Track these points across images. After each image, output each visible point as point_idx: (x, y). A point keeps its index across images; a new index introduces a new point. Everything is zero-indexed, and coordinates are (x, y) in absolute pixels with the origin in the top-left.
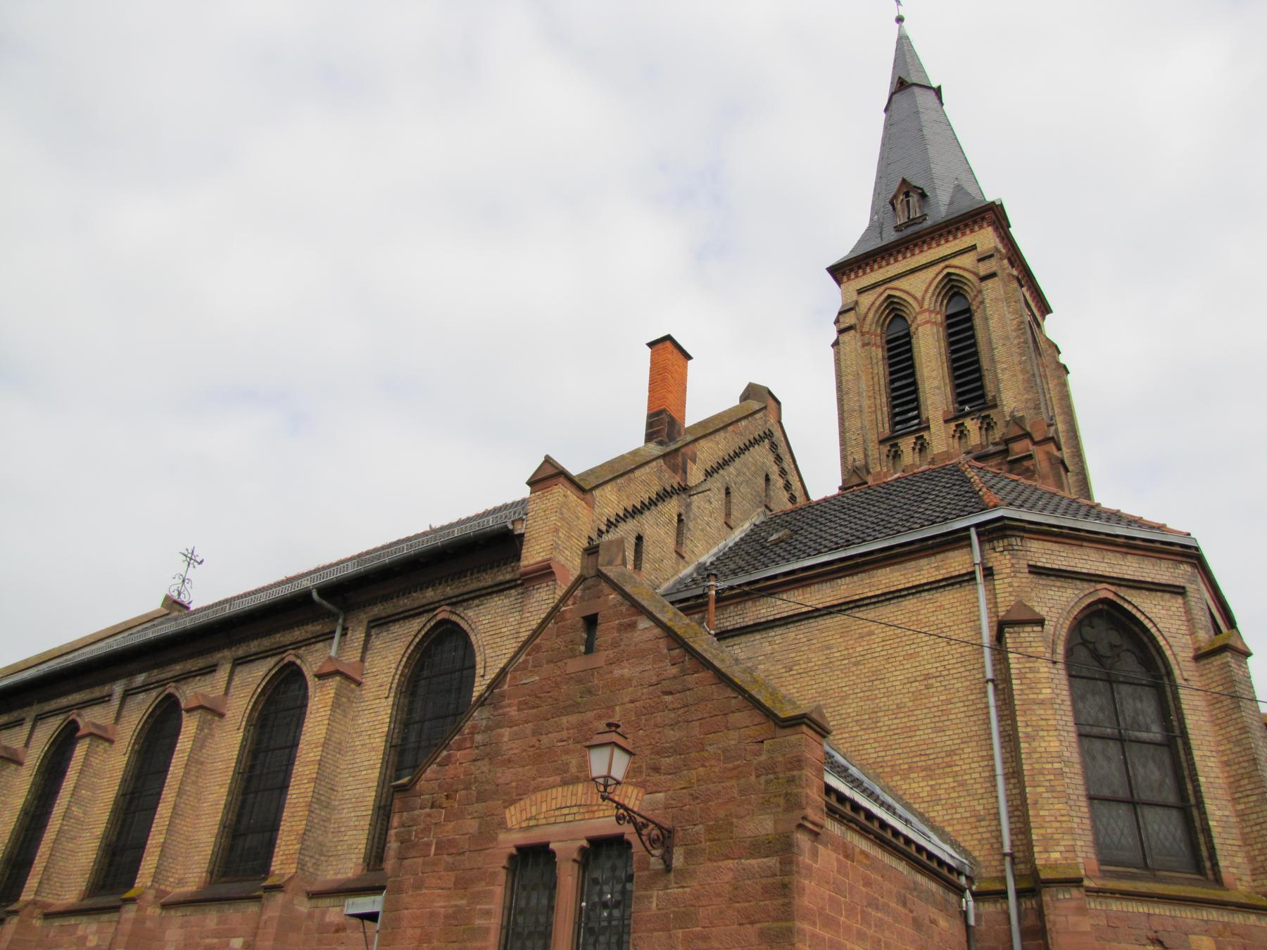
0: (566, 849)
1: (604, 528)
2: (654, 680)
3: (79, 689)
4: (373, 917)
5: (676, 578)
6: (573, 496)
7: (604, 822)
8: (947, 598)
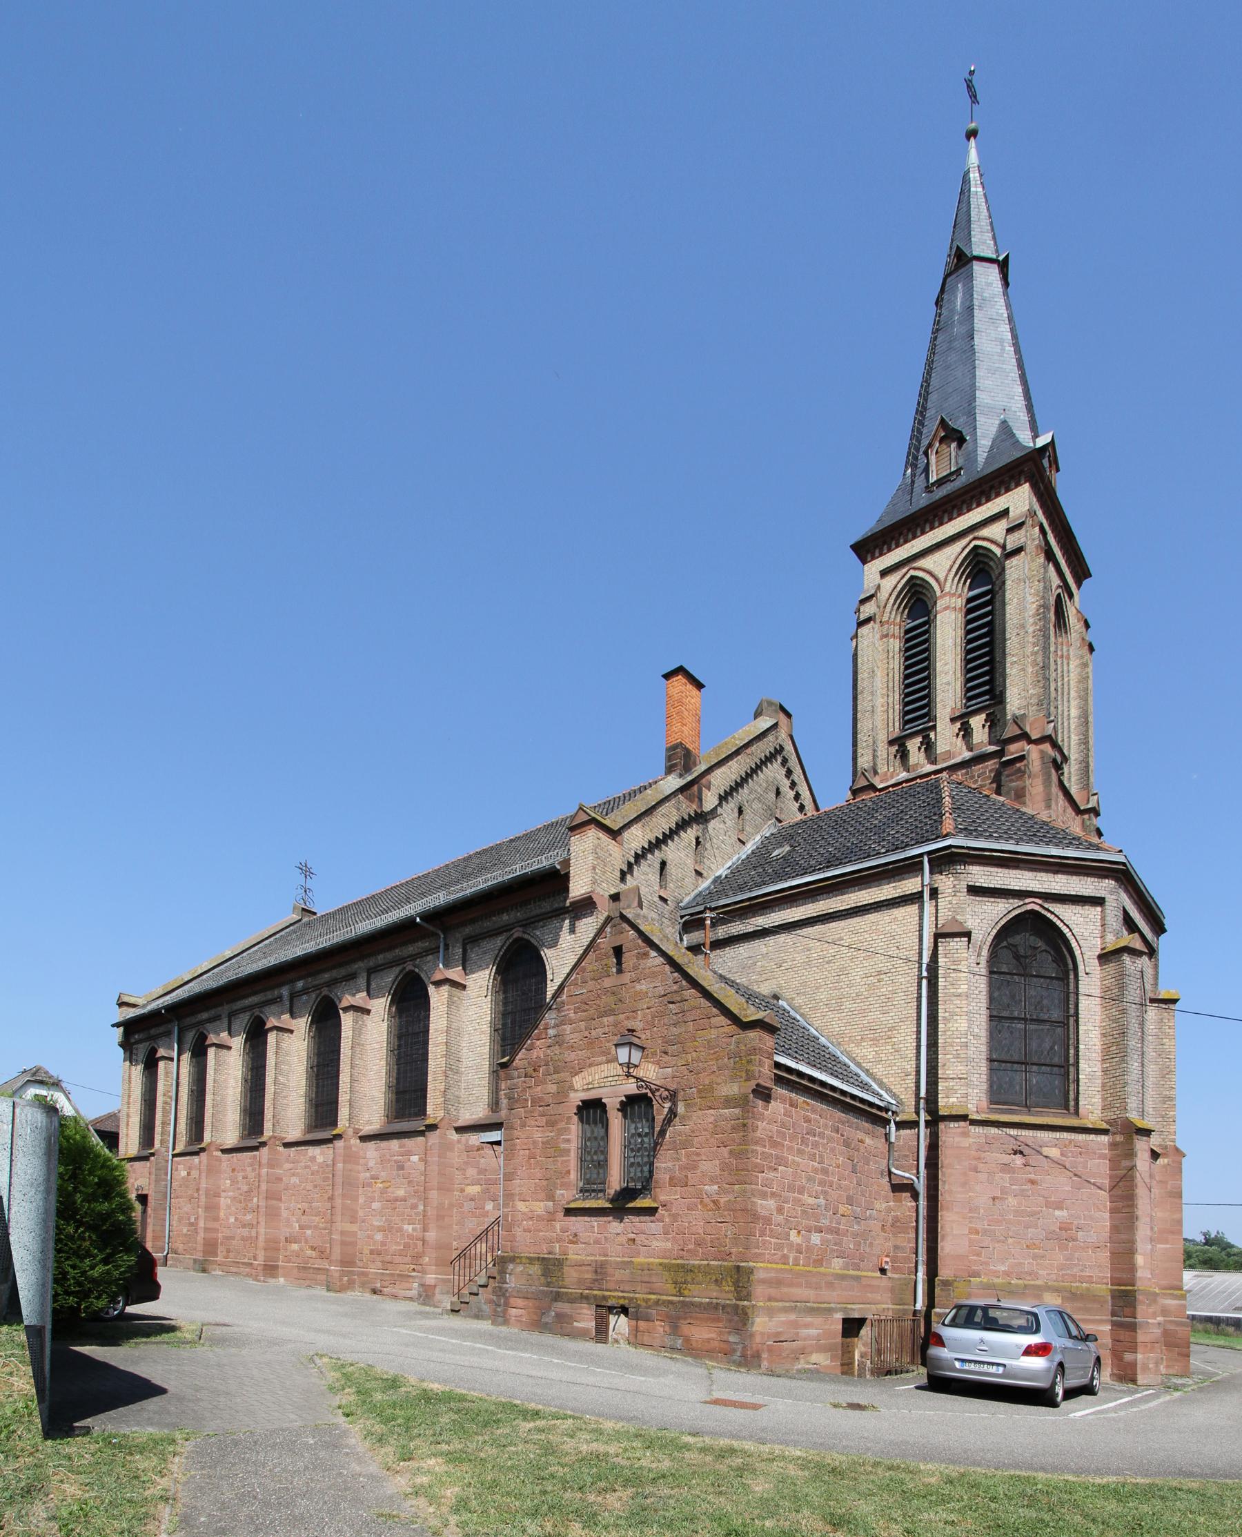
1: (632, 860)
3: (255, 993)
4: (498, 1143)
5: (696, 892)
7: (631, 1088)
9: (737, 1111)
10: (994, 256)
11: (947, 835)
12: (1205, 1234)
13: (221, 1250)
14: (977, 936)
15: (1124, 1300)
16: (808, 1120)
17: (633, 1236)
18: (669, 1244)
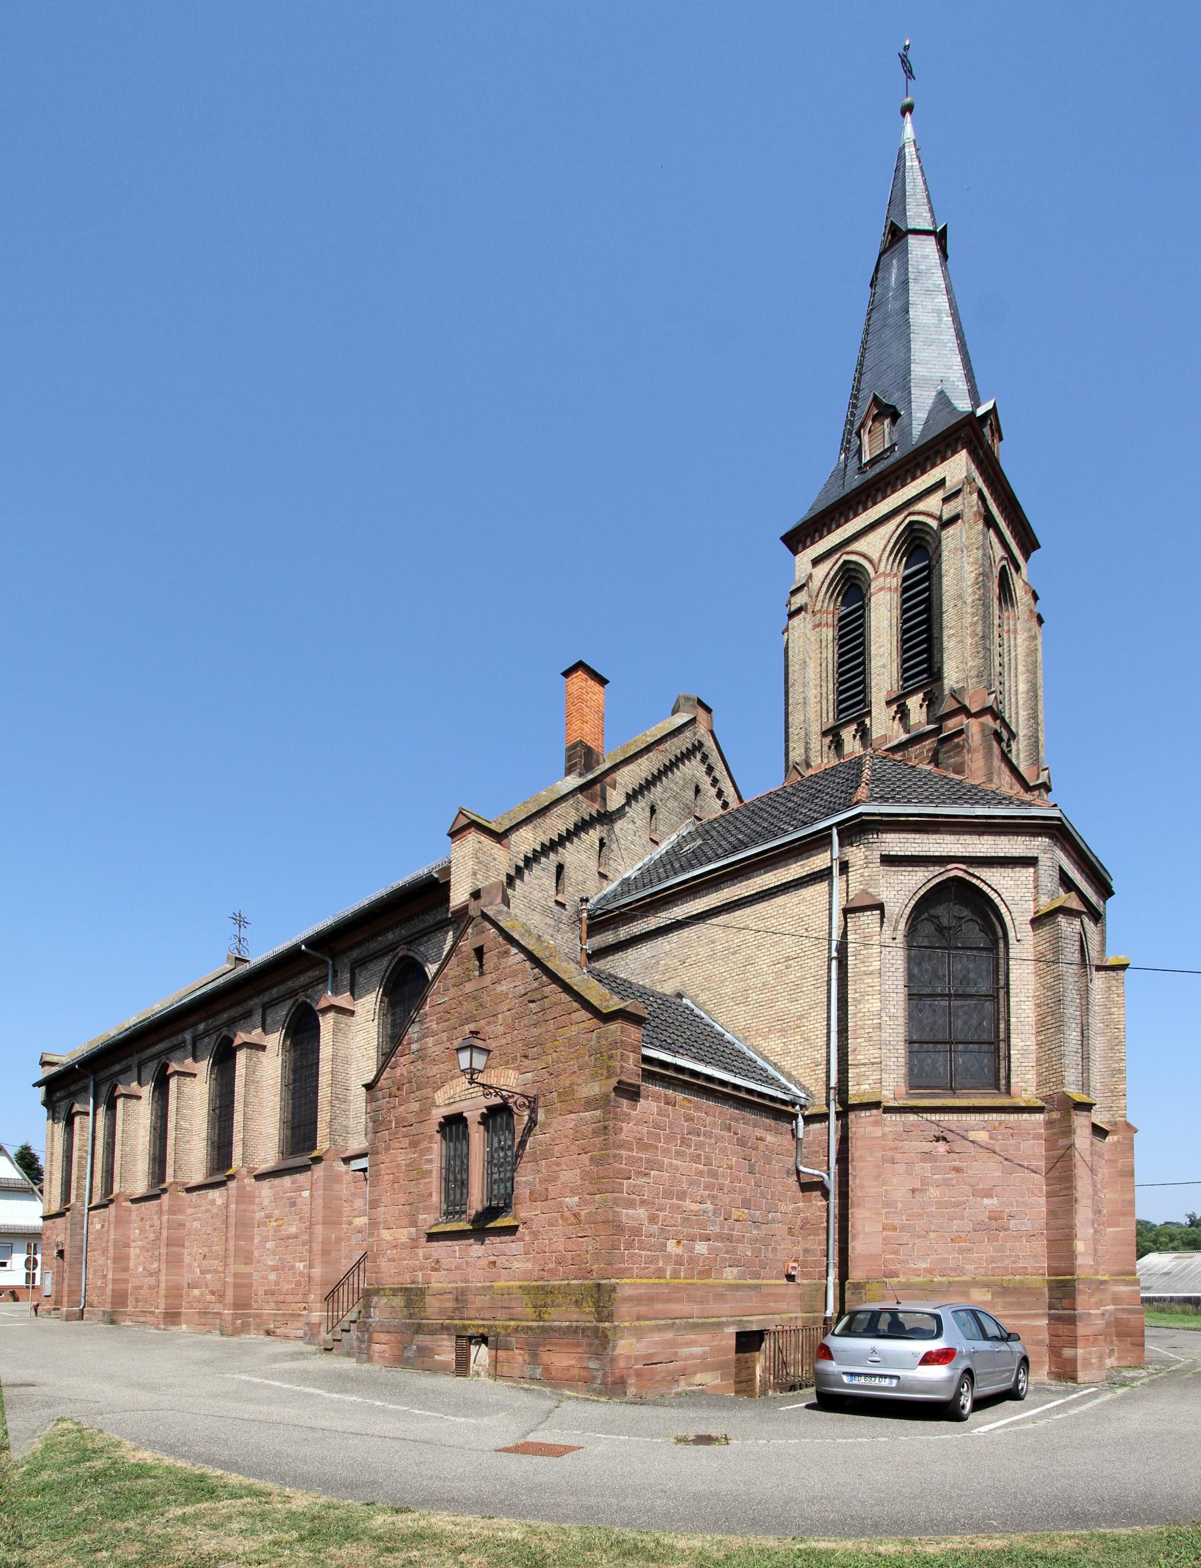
0: (473, 1117)
1: (522, 864)
2: (523, 992)
3: (161, 1040)
4: (364, 1170)
5: (600, 895)
6: (487, 841)
8: (808, 892)
9: (598, 1113)
10: (931, 228)
11: (857, 803)
12: (1190, 1217)
13: (131, 1300)
14: (892, 909)
15: (1062, 1291)
16: (689, 1119)
17: (493, 1258)
18: (529, 1265)
